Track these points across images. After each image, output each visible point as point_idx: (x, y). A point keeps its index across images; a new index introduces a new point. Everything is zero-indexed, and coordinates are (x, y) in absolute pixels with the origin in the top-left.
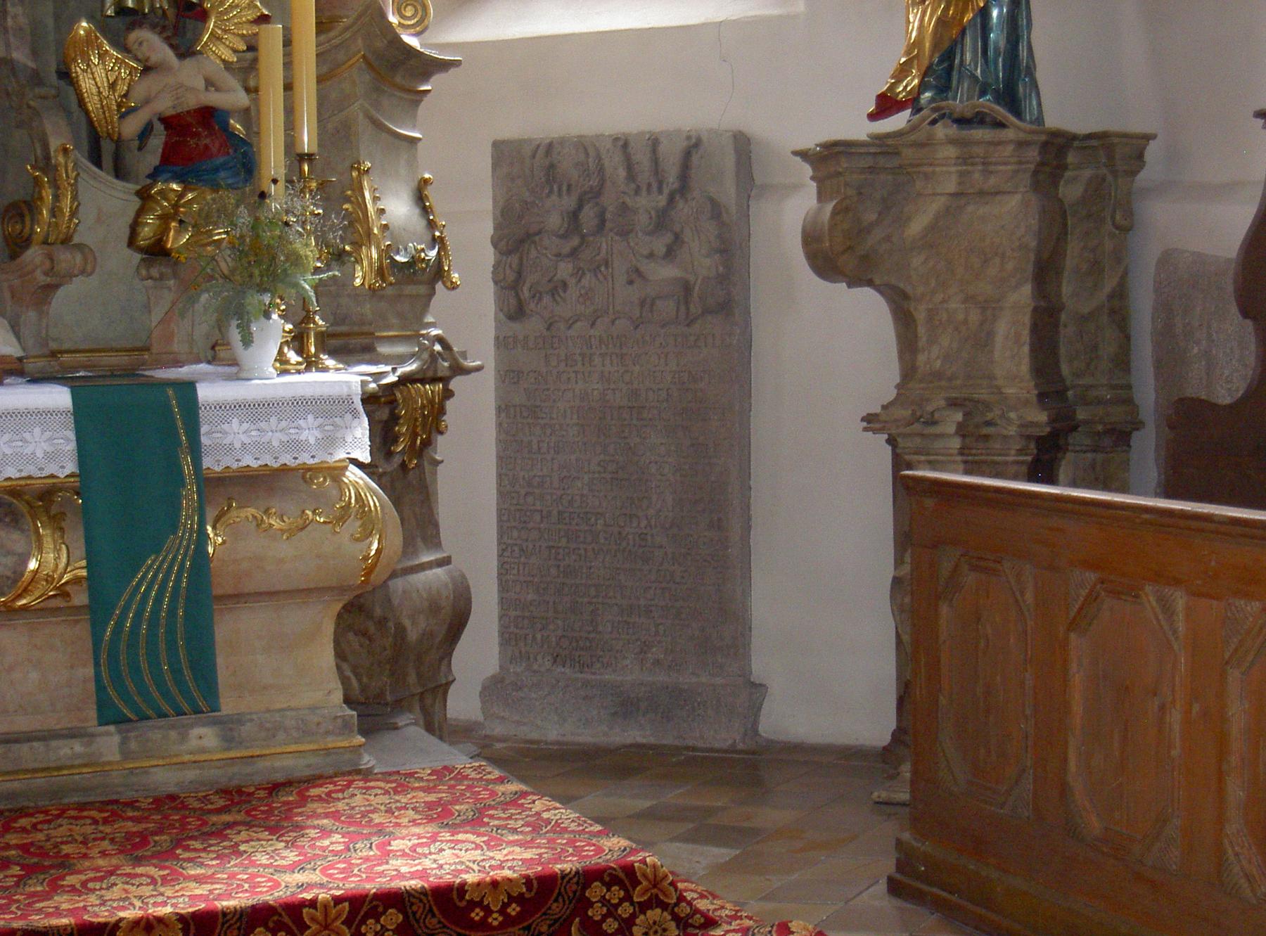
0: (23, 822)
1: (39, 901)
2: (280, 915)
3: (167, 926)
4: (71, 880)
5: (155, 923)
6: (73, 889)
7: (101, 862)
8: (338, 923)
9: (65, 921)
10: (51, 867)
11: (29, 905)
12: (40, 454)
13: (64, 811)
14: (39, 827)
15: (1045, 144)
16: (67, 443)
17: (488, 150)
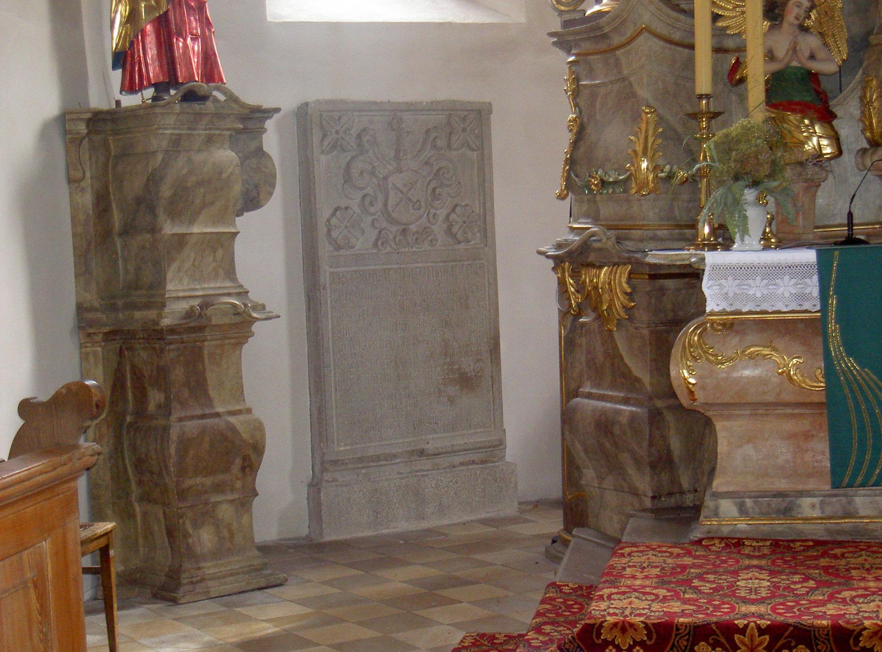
0: (838, 551)
1: (815, 607)
2: (717, 635)
3: (636, 630)
4: (846, 594)
5: (627, 626)
6: (844, 601)
7: (872, 584)
8: (760, 648)
9: (825, 622)
10: (836, 584)
11: (808, 608)
12: (787, 295)
13: (869, 547)
14: (846, 555)
15: (89, 121)
16: (813, 286)
17: (488, 100)
